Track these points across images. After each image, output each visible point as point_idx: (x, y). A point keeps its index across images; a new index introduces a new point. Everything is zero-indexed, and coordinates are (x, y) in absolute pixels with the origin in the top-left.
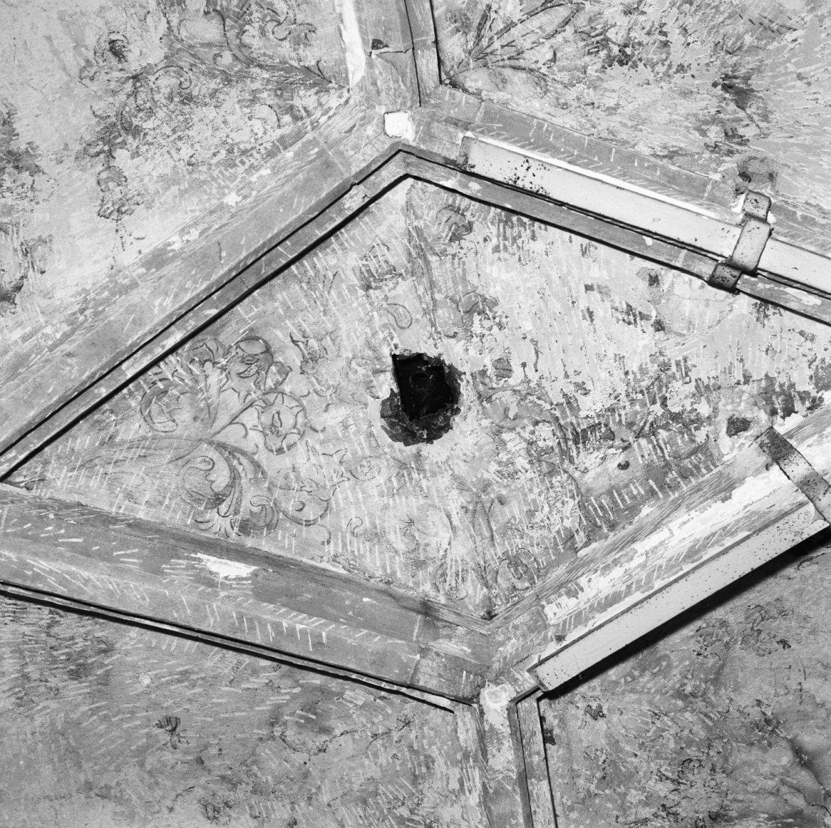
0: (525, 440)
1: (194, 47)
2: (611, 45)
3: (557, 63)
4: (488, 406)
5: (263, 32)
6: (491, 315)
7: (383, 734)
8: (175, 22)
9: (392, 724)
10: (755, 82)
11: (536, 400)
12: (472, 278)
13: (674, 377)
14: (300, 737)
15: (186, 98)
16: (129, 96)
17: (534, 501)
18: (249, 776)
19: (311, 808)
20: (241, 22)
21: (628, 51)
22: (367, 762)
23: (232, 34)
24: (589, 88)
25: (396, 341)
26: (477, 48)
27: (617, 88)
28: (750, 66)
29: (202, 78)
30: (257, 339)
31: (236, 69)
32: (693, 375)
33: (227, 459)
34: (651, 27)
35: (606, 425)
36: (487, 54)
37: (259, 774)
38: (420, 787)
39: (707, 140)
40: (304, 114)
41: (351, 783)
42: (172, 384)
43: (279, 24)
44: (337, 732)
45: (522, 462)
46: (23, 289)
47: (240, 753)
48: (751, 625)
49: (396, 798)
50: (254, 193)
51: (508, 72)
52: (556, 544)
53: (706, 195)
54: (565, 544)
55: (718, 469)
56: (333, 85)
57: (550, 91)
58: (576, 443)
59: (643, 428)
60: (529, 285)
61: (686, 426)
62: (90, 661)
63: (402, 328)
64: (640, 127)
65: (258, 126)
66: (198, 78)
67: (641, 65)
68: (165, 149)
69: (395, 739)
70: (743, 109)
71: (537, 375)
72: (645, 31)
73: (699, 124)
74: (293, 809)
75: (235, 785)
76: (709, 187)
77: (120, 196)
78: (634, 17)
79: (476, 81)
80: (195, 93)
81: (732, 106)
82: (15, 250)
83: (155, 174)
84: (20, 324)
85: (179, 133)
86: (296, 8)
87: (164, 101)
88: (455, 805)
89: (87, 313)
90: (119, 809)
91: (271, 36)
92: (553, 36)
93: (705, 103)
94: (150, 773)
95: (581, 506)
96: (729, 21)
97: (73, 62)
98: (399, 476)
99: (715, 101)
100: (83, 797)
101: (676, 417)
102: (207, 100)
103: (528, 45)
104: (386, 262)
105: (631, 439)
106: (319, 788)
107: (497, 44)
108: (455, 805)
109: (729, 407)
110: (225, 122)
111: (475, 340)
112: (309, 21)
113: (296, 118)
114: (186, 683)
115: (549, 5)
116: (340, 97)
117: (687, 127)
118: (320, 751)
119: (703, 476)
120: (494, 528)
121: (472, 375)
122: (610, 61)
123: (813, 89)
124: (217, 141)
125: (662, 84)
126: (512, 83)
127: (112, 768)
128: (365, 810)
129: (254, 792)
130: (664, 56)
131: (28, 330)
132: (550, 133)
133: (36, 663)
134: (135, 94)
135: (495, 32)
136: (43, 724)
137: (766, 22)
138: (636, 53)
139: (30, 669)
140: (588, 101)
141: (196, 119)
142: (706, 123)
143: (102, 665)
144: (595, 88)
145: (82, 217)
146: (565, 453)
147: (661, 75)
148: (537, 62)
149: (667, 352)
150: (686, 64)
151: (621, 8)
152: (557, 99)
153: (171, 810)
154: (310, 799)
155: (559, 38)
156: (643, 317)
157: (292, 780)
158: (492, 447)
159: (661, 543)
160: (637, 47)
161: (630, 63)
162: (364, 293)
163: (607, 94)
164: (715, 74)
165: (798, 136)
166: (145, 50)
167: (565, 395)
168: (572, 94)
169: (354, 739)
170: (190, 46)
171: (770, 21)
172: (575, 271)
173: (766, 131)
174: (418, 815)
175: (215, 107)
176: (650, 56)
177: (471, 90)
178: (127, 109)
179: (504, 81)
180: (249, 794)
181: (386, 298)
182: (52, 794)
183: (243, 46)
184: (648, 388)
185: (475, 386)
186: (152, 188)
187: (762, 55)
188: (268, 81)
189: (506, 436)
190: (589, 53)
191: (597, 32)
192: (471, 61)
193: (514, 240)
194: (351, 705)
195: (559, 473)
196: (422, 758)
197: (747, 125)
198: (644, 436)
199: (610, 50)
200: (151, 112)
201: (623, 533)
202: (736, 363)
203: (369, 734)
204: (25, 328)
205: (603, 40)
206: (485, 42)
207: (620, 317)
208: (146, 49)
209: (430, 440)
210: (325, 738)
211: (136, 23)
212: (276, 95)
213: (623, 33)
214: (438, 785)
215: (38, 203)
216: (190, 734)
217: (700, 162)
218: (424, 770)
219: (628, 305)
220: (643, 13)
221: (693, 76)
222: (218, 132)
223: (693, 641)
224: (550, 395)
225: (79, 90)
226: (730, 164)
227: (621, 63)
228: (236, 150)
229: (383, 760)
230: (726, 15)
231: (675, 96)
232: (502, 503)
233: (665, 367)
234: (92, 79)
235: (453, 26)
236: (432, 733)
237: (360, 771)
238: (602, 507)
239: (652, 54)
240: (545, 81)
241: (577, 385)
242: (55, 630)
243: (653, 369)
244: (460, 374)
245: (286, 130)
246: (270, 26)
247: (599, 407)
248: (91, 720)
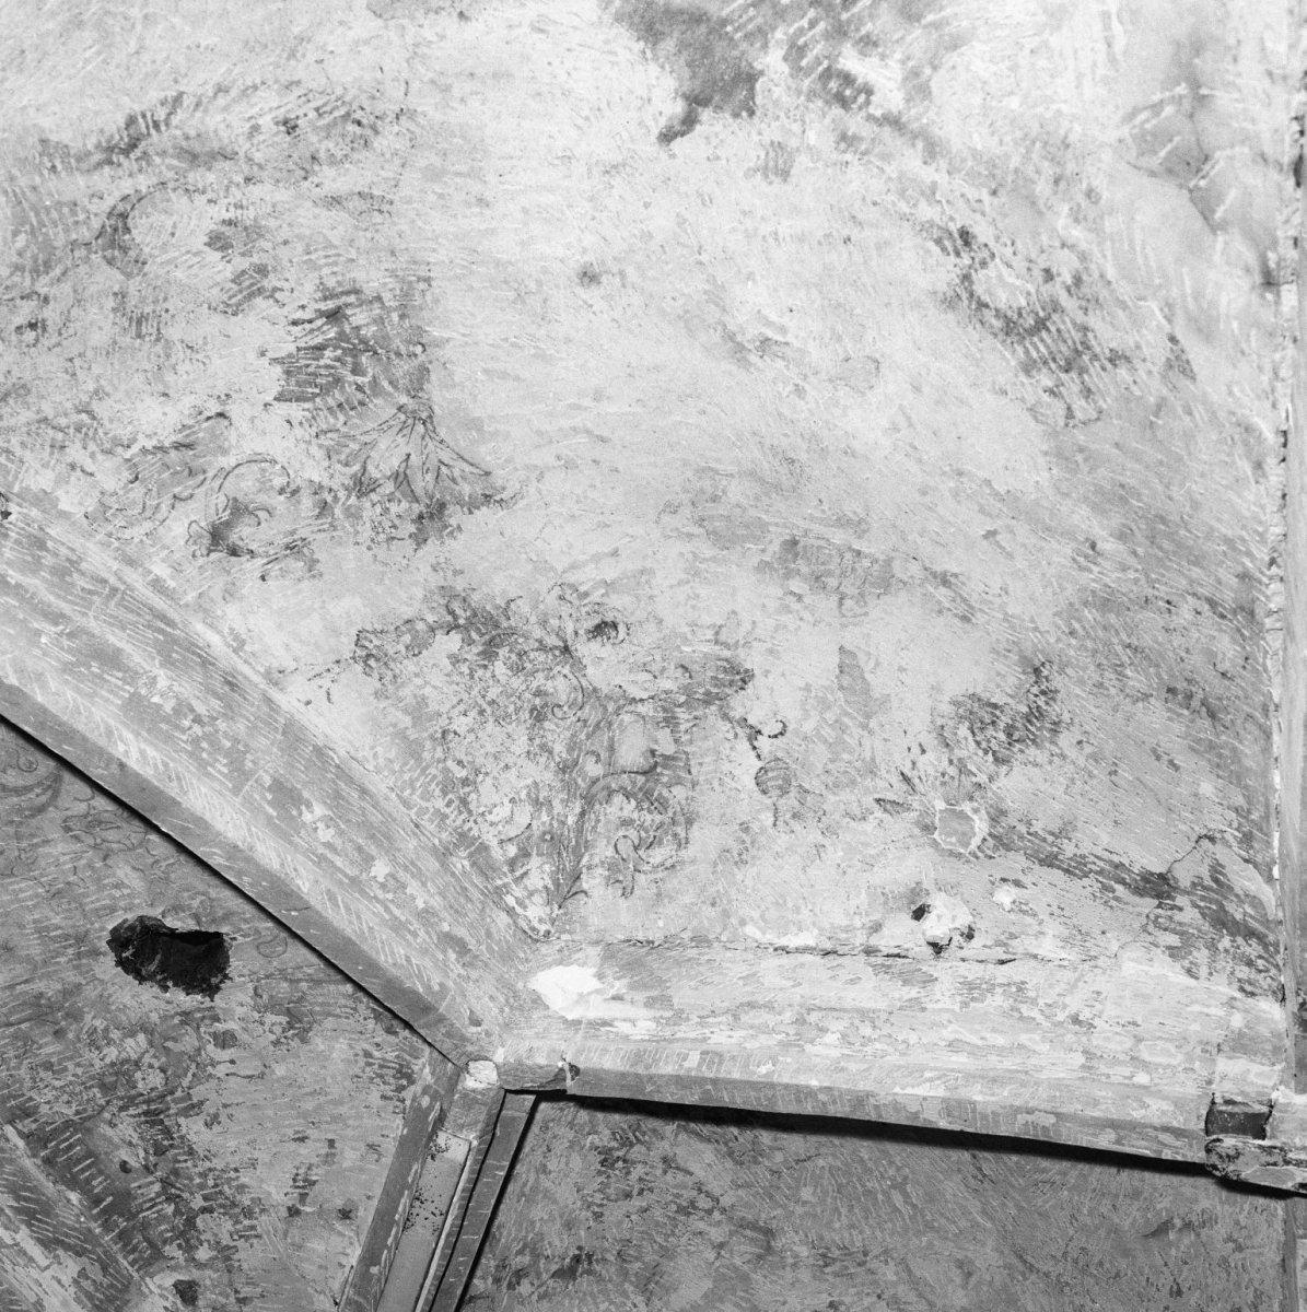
0: (140, 1058)
1: (609, 728)
4: (176, 1021)
5: (626, 823)
8: (641, 708)
12: (329, 1023)
13: (237, 1222)
15: (539, 713)
16: (540, 641)
17: (66, 1069)
20: (640, 795)
23: (625, 780)
29: (568, 734)
31: (579, 780)
32: (241, 1243)
33: (39, 784)
35: (171, 1146)
40: (518, 874)
43: (636, 848)
45: (112, 1054)
46: (233, 559)
50: (390, 896)
52: (15, 1097)
54: (17, 1107)
55: (135, 1274)
56: (556, 911)
58: (146, 1113)
59: (173, 1186)
60: (329, 1080)
61: (182, 1234)
65: (503, 812)
66: (568, 729)
68: (465, 696)
77: (391, 652)
80: (547, 724)
81: (554, 1267)
82: (293, 533)
83: (427, 691)
84: (177, 569)
85: (489, 710)
86: (653, 876)
87: (534, 685)
89: (197, 729)
91: (621, 833)
95: (68, 1124)
97: (586, 577)
98: (67, 937)
99: (560, 1251)
101: (190, 1223)
102: (537, 741)
109: (208, 1282)
110: (507, 767)
111: (256, 1015)
112: (637, 892)
113: (512, 863)
116: (540, 921)
119: (125, 1258)
120: (23, 1026)
124: (480, 761)
131: (171, 584)
134: (542, 647)
141: (510, 729)
145: (352, 611)
146: (131, 1101)
149: (264, 1217)
156: (303, 1197)
158: (125, 1022)
159: (31, 1259)
166: (604, 664)
167: (202, 1103)
170: (610, 724)
172: (350, 1132)
178: (521, 640)
183: (610, 793)
184: (221, 1192)
185: (199, 1010)
186: (406, 692)
188: (563, 823)
189: (141, 1037)
193: (381, 1076)
195: (104, 1095)
200: (517, 669)
201: (42, 1177)
202: (259, 1290)
204: (173, 578)
207: (301, 1171)
208: (604, 665)
209: (120, 962)
211: (641, 658)
212: (544, 833)
215: (369, 548)
219: (315, 1182)
220: (665, 1172)
222: (491, 760)
224: (201, 1087)
225: (543, 584)
228: (467, 789)
232: (56, 1033)
233: (248, 1213)
234: (561, 598)
238: (71, 1147)
243: (246, 1200)
245: (497, 853)
246: (632, 833)
247: (192, 1137)
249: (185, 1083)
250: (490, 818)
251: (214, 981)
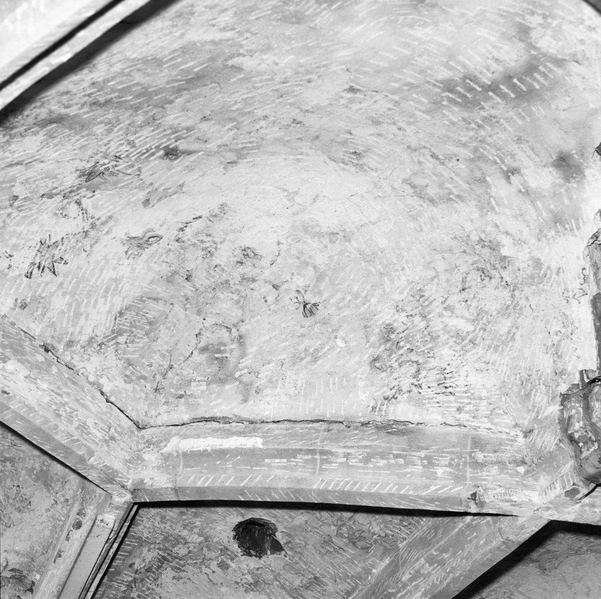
6: (245, 585)
7: (167, 372)
9: (165, 383)
14: (217, 335)
18: (237, 290)
19: (183, 294)
22: (166, 348)
30: (362, 549)
35: (154, 572)
37: (230, 295)
38: (122, 362)
41: (167, 328)
42: (399, 525)
44: (196, 353)
45: (185, 533)
47: (251, 304)
48: (5, 513)
49: (132, 342)
58: (163, 557)
59: (135, 584)
62: (383, 347)
69: (158, 376)
71: (204, 571)
74: (194, 286)
75: (243, 279)
88: (94, 370)
90: (317, 229)
94: (306, 264)
100: (348, 230)
104: (312, 591)
105: (137, 576)
106: (186, 309)
108: (94, 370)
111: (246, 572)
114: (311, 350)
118: (200, 333)
127: (336, 258)
128: (147, 319)
129: (227, 282)
133: (419, 330)
136: (399, 279)
139: (423, 325)
143: (372, 346)
153: (279, 243)
154: (187, 299)
157: (207, 303)
167: (184, 571)
169: (183, 355)
174: (112, 345)
180: (230, 278)
181: (303, 575)
182: (371, 227)
185: (232, 552)
194: (198, 378)
196: (134, 378)
198: (132, 581)
203: (175, 366)
210: (202, 344)
214: (114, 372)
216: (292, 308)
218: (128, 373)
223: (28, 494)
229: (157, 357)
236: (138, 396)
237: (166, 339)
241: (181, 578)
242: (414, 369)
248: (365, 292)
249: (189, 562)
251: (252, 552)
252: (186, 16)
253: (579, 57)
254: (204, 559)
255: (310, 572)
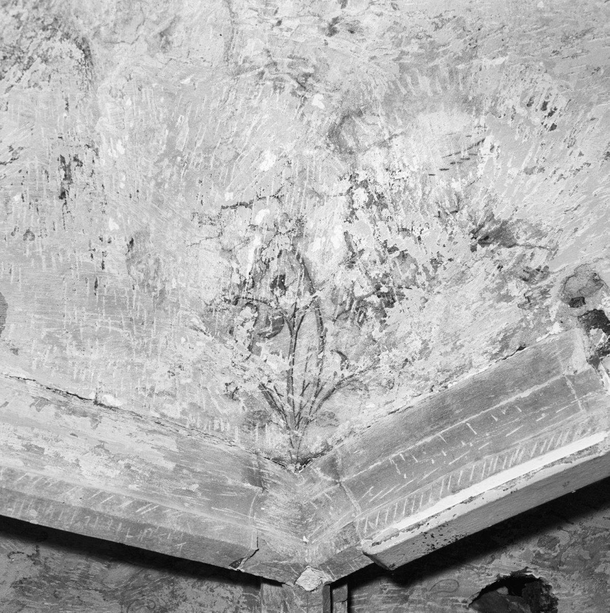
2: (368, 300)
3: (349, 357)
8: (99, 587)
10: (501, 214)
11: (593, 537)
21: (384, 289)
24: (390, 350)
25: (460, 599)
26: (289, 418)
27: (409, 328)
28: (482, 204)
29: (155, 593)
34: (379, 255)
36: (299, 413)
39: (517, 301)
51: (327, 406)
53: (574, 392)
57: (368, 384)
63: (455, 590)
64: (458, 343)
67: (405, 291)
70: (515, 244)
72: (378, 262)
73: (496, 294)
76: (569, 383)
78: (358, 262)
79: (315, 440)
80: (163, 604)
81: (505, 251)
92: (323, 343)
93: (482, 269)
96: (427, 189)
99: (487, 260)
102: (175, 601)
103: (315, 371)
107: (297, 399)
110: (201, 605)
115: (295, 329)
117: (491, 306)
121: (532, 563)
122: (381, 312)
123: (549, 171)
125: (436, 289)
126: (338, 410)
130: (413, 267)
132: (410, 457)
135: (286, 393)
137: (454, 158)
138: (391, 285)
140: (401, 361)
142: (500, 287)
144: (394, 345)
147: (427, 283)
148: (335, 374)
150: (435, 256)
151: (343, 267)
152: (380, 384)
155: (329, 339)
160: (387, 280)
161: (396, 298)
162: (407, 604)
163: (408, 341)
164: (464, 241)
165: (580, 222)
168: (384, 367)
170: (125, 587)
171: (456, 154)
173: (552, 246)
175: (184, 601)
176: (403, 278)
177: (320, 451)
179: (332, 416)
187: (480, 186)
190: (361, 323)
191: (348, 302)
192: (296, 432)
197: (533, 255)
199: (371, 304)
205: (358, 303)
206: (288, 408)
213: (365, 282)
217: (532, 326)
220: (362, 252)
221: (450, 260)
226: (555, 304)
227: (390, 304)
230: (420, 186)
231: (455, 288)
235: (256, 429)
239: (403, 274)
240: (356, 380)
244: (525, 570)
250: (230, 596)
252: (11, 474)
253: (126, 17)
254: (584, 543)
255: (420, 602)
